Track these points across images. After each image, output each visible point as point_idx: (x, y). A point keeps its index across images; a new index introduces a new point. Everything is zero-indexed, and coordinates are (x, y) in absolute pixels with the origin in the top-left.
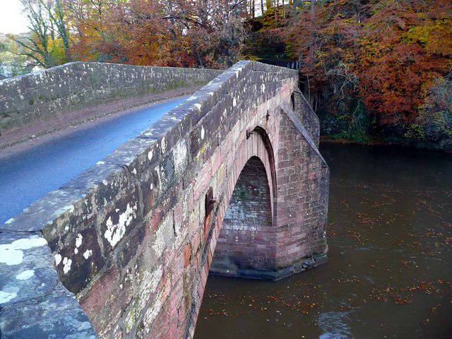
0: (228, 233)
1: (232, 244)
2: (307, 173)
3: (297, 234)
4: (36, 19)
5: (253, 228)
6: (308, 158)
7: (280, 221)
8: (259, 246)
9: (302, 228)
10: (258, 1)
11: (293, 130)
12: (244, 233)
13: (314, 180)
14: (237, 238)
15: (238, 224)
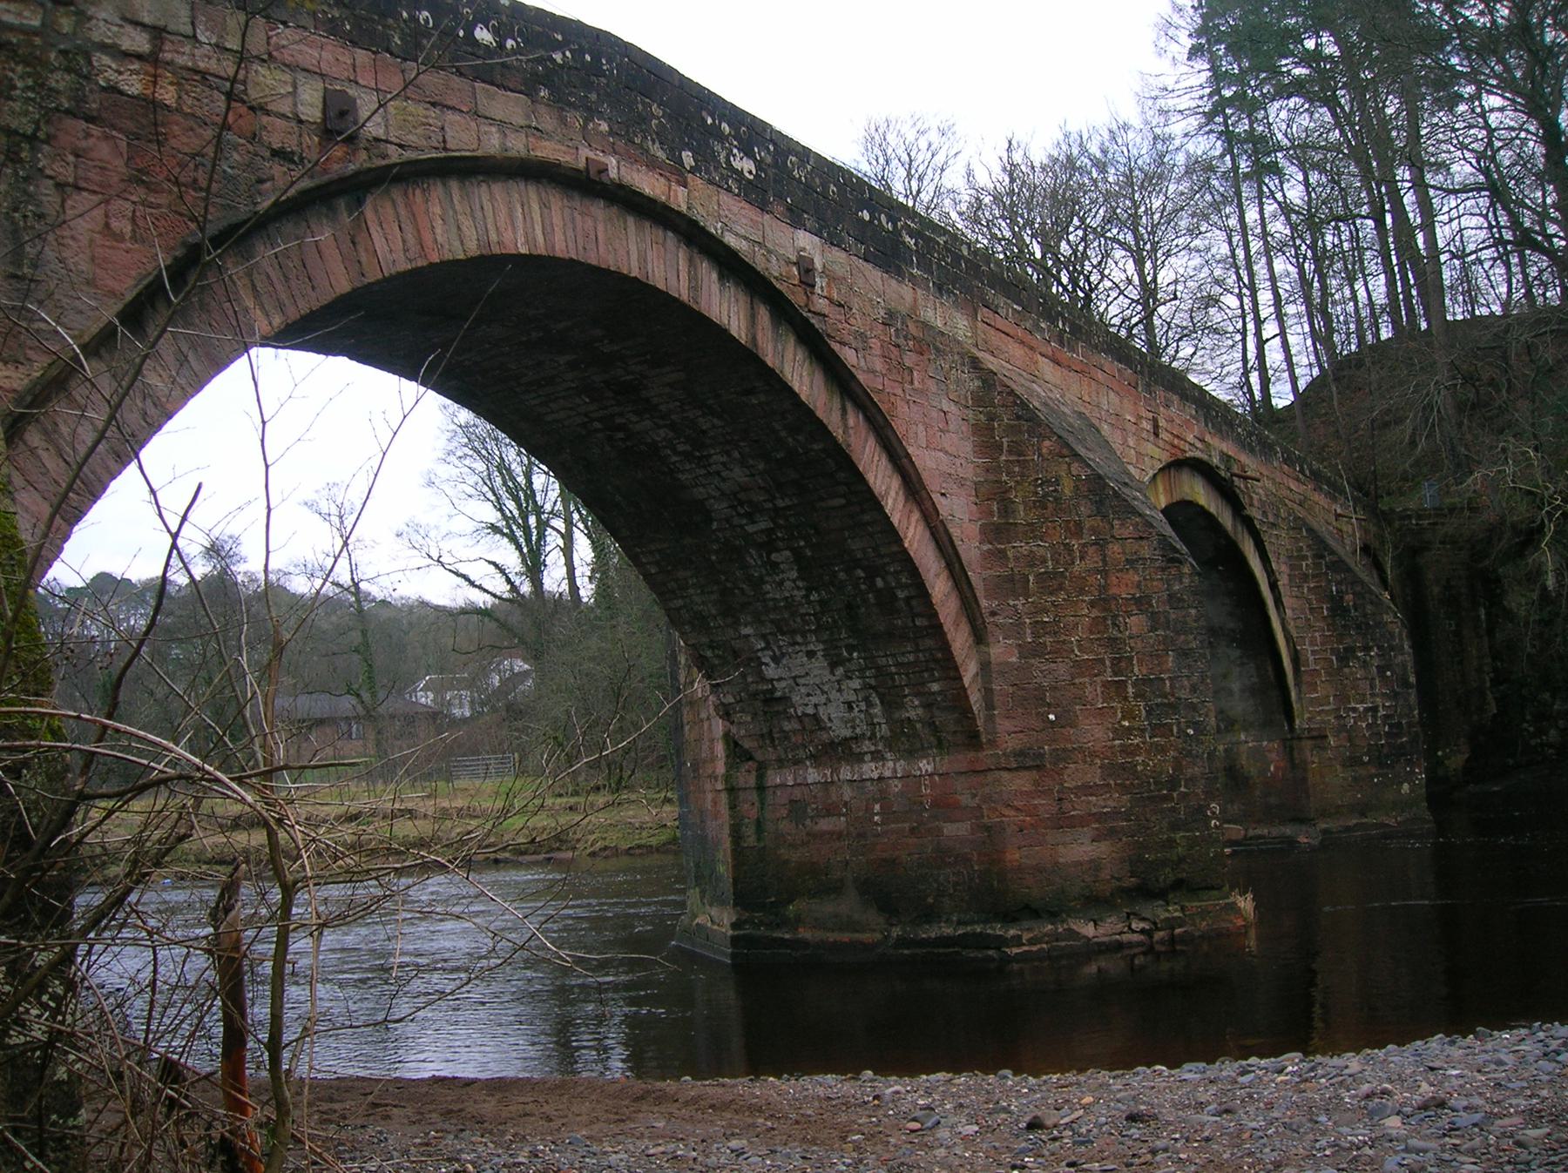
0: (847, 793)
1: (861, 835)
2: (1105, 573)
3: (1087, 789)
4: (516, 499)
5: (925, 766)
6: (1097, 521)
7: (1008, 733)
8: (949, 829)
9: (1111, 770)
10: (3, 939)
11: (1025, 425)
12: (896, 787)
13: (1138, 602)
14: (877, 807)
15: (877, 756)
